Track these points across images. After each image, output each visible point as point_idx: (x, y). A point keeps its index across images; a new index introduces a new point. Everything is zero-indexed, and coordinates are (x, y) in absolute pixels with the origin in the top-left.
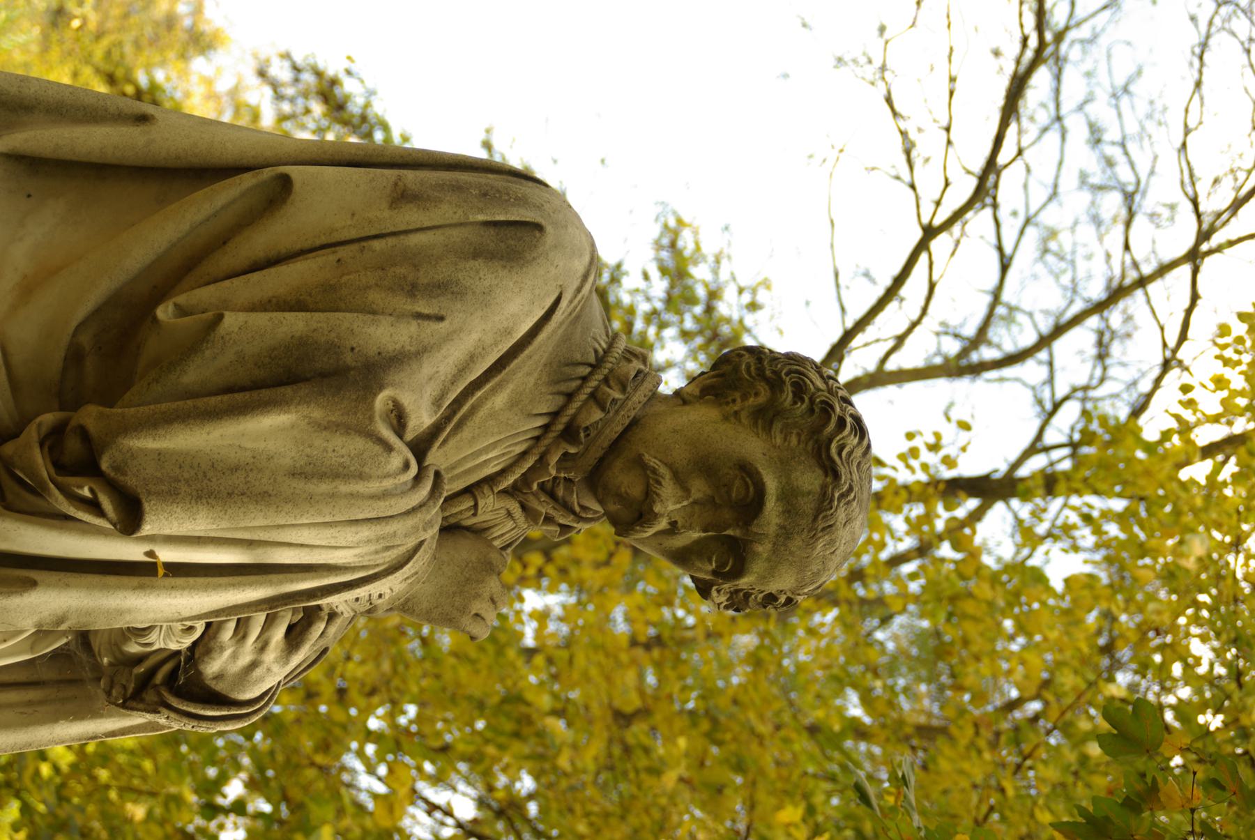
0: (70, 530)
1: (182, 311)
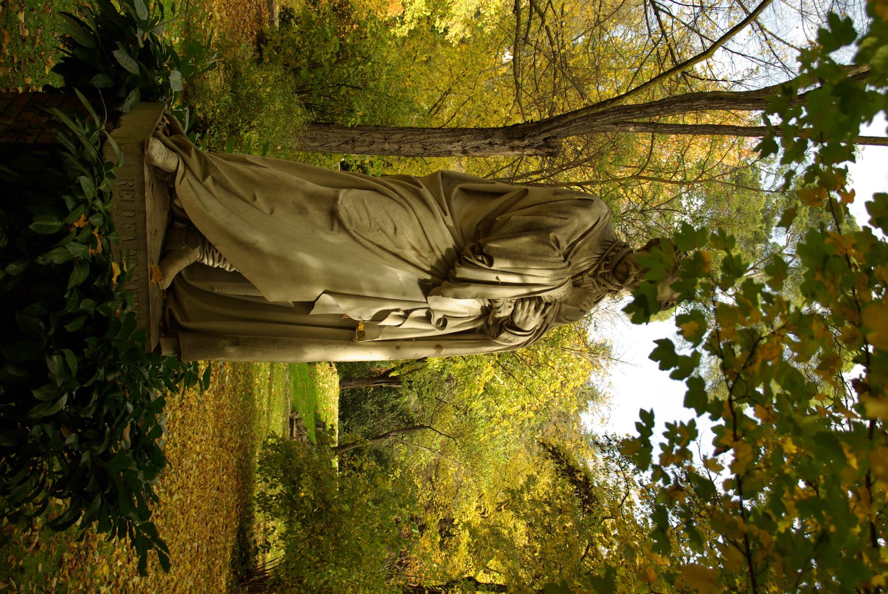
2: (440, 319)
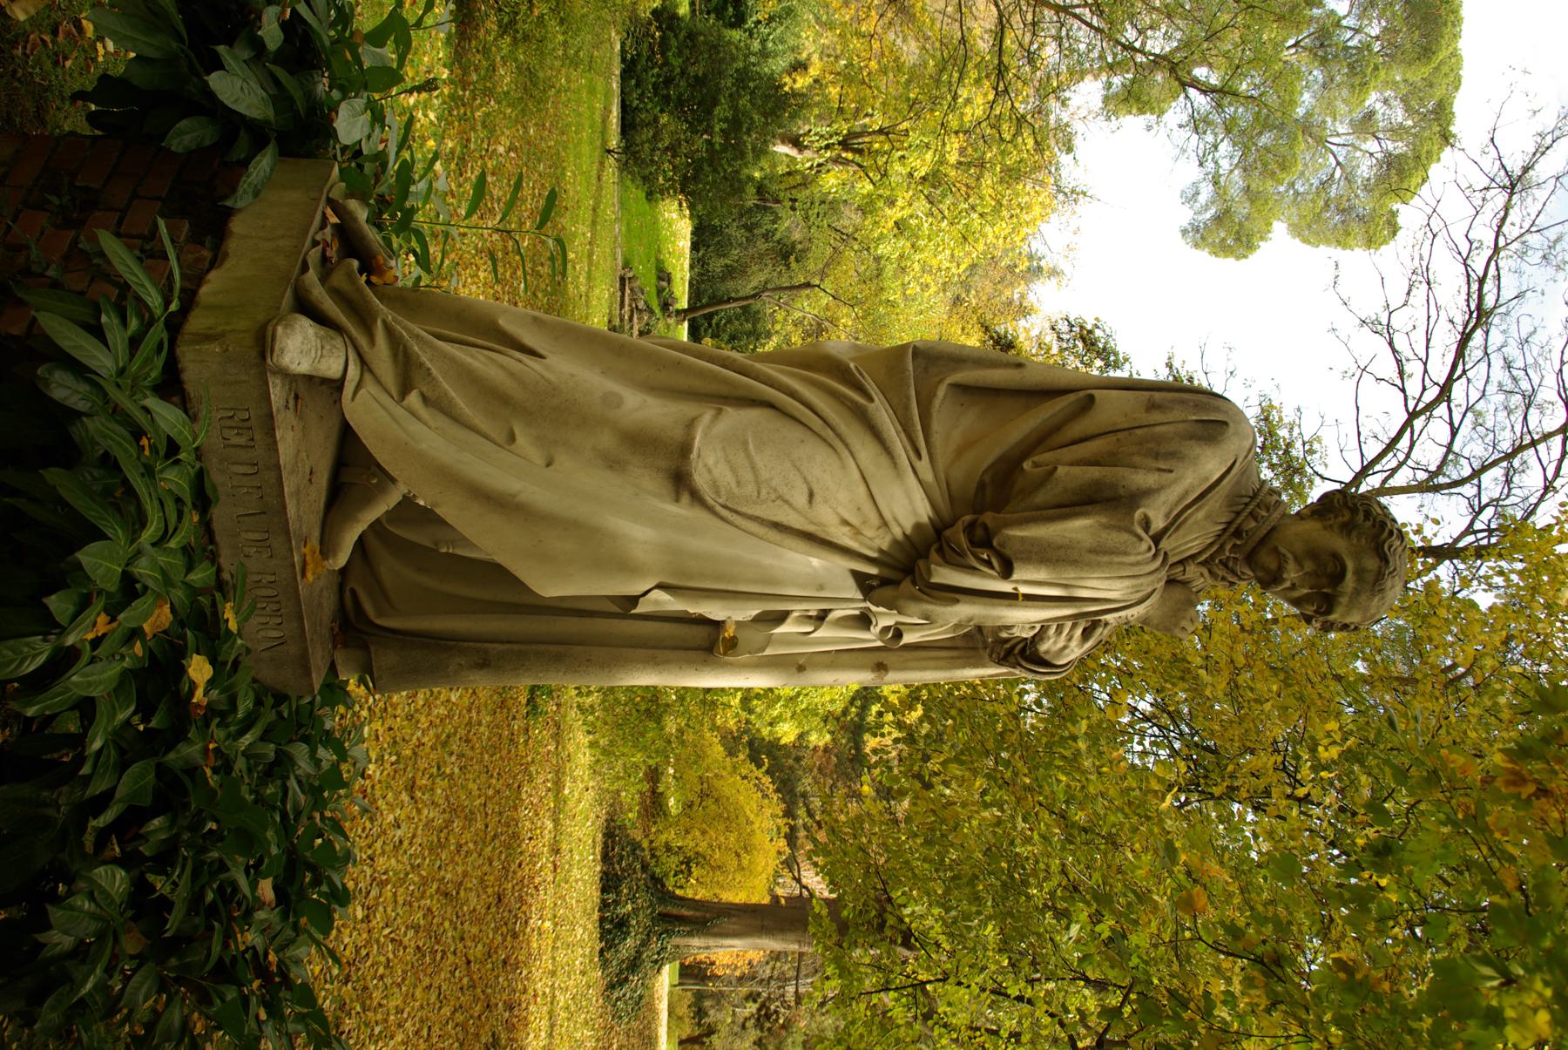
0: (973, 574)
1: (1036, 465)
2: (890, 627)
